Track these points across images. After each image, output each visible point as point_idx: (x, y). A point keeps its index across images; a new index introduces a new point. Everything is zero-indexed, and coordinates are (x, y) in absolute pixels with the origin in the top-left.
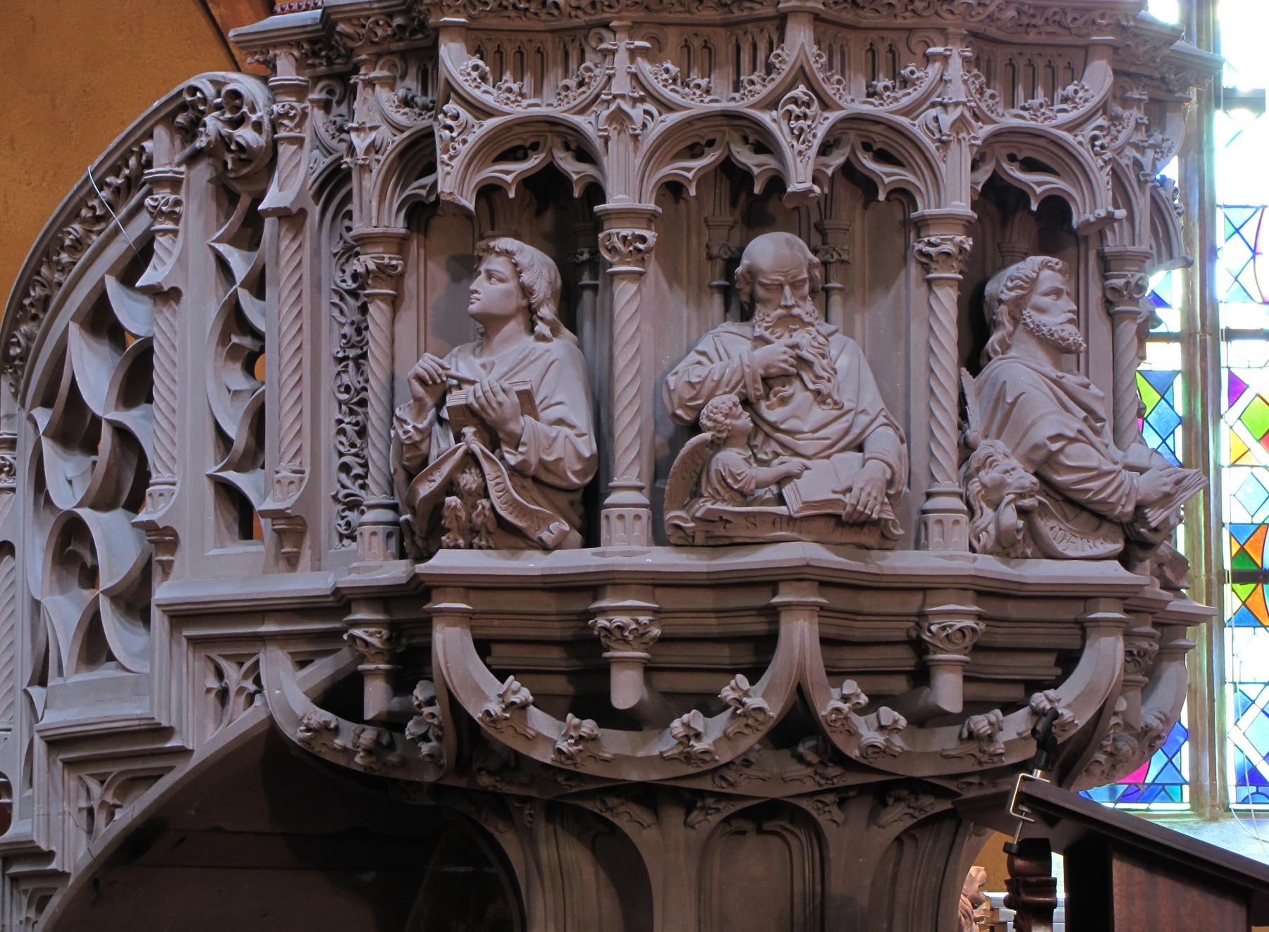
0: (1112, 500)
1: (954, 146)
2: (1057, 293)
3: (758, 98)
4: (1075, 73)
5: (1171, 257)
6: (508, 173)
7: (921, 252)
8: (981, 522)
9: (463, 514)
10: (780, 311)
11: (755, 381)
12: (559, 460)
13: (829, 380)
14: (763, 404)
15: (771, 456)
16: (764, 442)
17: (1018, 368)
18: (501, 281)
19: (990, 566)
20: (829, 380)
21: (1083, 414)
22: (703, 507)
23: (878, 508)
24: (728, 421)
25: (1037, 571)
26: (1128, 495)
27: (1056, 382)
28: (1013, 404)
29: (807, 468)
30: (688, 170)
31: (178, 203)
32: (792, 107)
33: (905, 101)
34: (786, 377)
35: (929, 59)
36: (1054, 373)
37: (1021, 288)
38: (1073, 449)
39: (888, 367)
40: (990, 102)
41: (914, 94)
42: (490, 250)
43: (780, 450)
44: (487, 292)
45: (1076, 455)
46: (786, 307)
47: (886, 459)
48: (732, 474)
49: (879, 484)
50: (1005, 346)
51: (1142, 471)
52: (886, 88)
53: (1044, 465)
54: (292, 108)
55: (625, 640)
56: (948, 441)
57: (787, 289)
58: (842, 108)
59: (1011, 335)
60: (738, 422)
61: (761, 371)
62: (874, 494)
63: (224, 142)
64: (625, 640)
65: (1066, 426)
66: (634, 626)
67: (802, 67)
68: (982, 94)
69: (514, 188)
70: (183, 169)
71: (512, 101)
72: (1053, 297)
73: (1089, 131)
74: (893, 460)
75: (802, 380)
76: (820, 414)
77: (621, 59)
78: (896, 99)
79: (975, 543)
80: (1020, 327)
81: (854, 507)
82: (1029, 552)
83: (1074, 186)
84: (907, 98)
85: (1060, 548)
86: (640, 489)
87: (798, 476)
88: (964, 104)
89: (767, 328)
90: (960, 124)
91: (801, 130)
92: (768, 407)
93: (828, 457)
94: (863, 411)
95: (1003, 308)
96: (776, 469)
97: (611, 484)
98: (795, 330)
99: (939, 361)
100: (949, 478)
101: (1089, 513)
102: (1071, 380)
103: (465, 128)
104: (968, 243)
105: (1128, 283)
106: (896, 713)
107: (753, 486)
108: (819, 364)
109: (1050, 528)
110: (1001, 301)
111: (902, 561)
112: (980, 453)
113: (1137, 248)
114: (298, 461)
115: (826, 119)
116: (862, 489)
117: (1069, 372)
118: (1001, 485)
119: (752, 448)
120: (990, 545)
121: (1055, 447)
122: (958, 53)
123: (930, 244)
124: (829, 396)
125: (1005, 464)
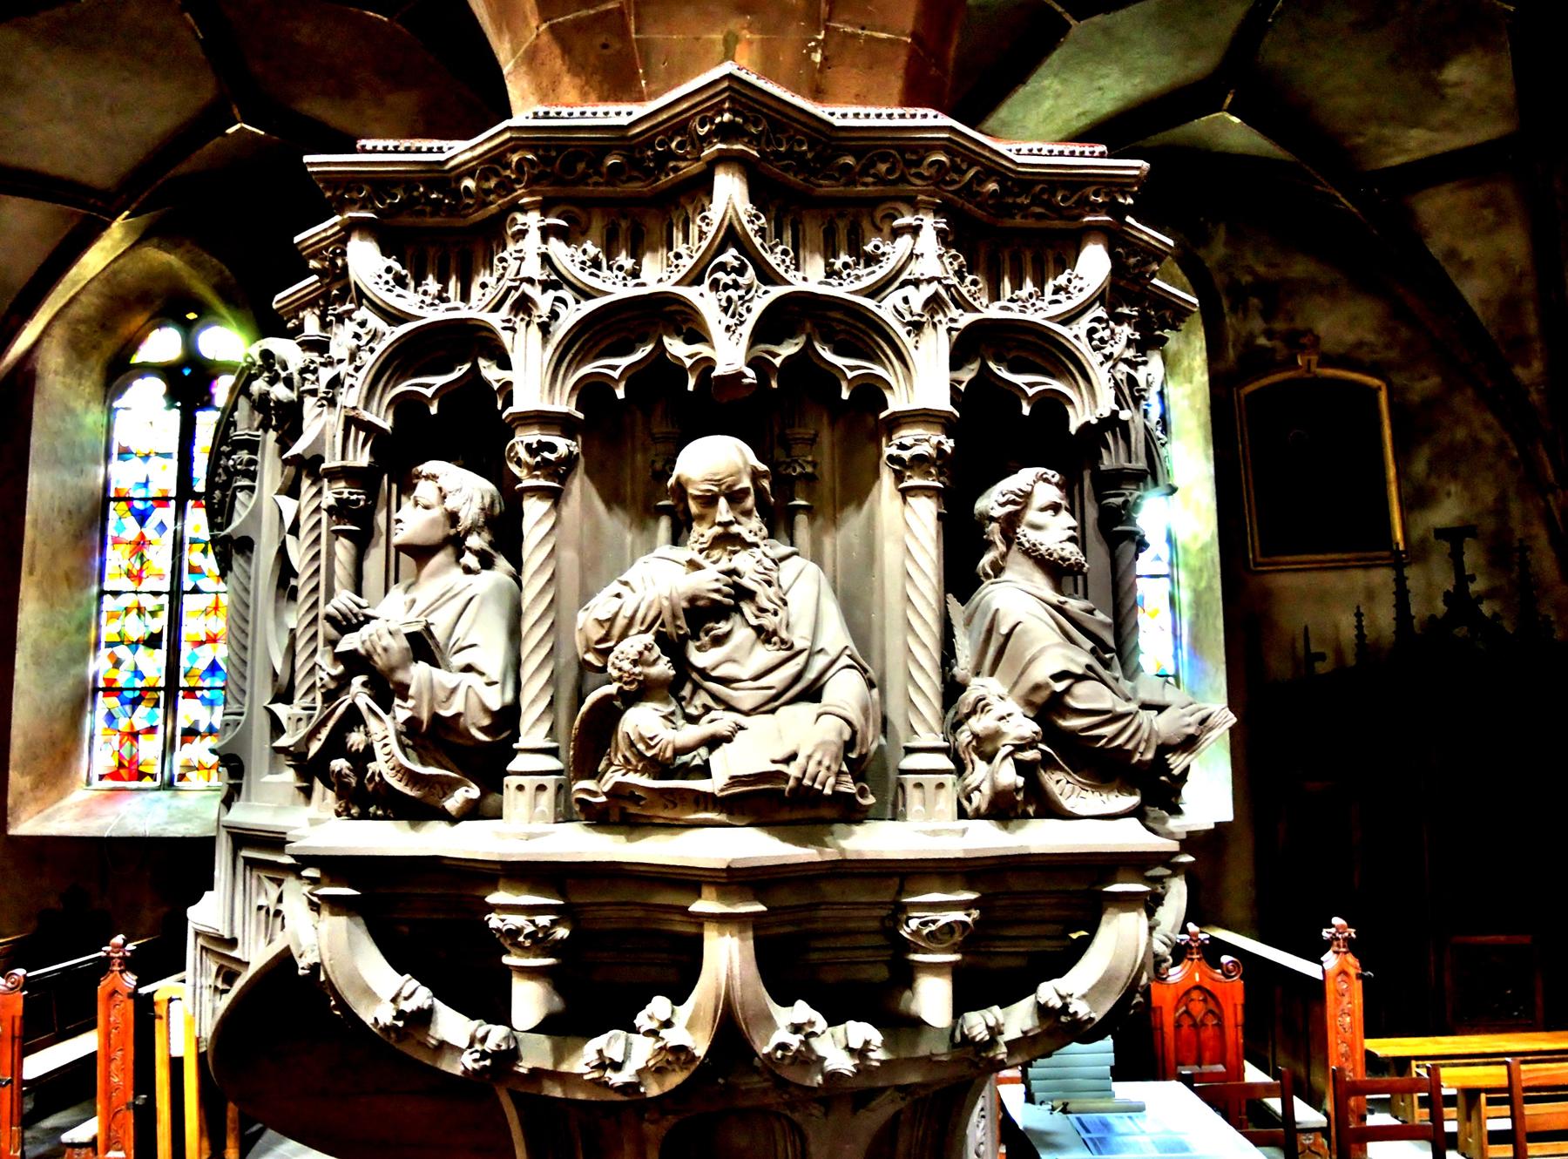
0: (1130, 746)
1: (928, 330)
2: (1055, 508)
3: (684, 271)
4: (1066, 260)
5: (1156, 483)
6: (428, 386)
7: (891, 458)
8: (972, 779)
9: (353, 781)
10: (718, 530)
11: (675, 616)
12: (459, 715)
13: (776, 613)
14: (692, 646)
15: (701, 710)
16: (694, 693)
17: (1015, 595)
18: (427, 508)
19: (987, 839)
20: (776, 613)
21: (1089, 645)
22: (613, 777)
23: (831, 781)
24: (638, 670)
25: (1038, 837)
26: (1148, 741)
27: (1059, 609)
28: (1008, 636)
29: (742, 728)
30: (614, 368)
31: (254, 462)
32: (720, 275)
33: (867, 281)
34: (719, 611)
35: (896, 233)
36: (1055, 598)
37: (1013, 502)
38: (1081, 689)
39: (856, 601)
40: (973, 288)
41: (880, 272)
42: (418, 476)
43: (711, 703)
44: (413, 520)
45: (1088, 695)
46: (720, 524)
47: (843, 713)
48: (642, 738)
49: (834, 749)
50: (998, 569)
51: (1161, 708)
52: (846, 266)
53: (1048, 707)
54: (313, 362)
55: (520, 946)
56: (930, 683)
57: (723, 502)
58: (789, 283)
59: (1004, 556)
60: (654, 671)
61: (685, 604)
62: (826, 762)
63: (265, 396)
64: (520, 946)
65: (1072, 660)
66: (530, 928)
67: (731, 225)
68: (962, 279)
69: (436, 403)
70: (260, 432)
71: (425, 304)
72: (1050, 512)
73: (1084, 324)
74: (855, 715)
75: (742, 615)
76: (766, 655)
77: (534, 236)
78: (858, 278)
79: (965, 803)
80: (1015, 547)
81: (799, 780)
82: (1031, 810)
83: (1071, 386)
84: (870, 276)
85: (1068, 804)
86: (553, 752)
87: (728, 739)
88: (939, 280)
89: (701, 551)
90: (934, 304)
91: (729, 300)
92: (699, 649)
93: (773, 711)
94: (821, 651)
95: (994, 527)
96: (703, 729)
97: (515, 746)
98: (735, 552)
99: (916, 587)
100: (931, 730)
101: (1103, 765)
102: (1075, 605)
103: (375, 336)
104: (949, 445)
105: (1126, 502)
106: (1097, 19)
107: (669, 754)
108: (764, 595)
109: (1060, 785)
110: (992, 519)
111: (870, 841)
112: (969, 696)
113: (1134, 465)
114: (310, 698)
115: (766, 292)
116: (809, 757)
117: (1070, 596)
118: (997, 735)
119: (680, 700)
120: (984, 807)
121: (1059, 687)
122: (930, 224)
123: (902, 447)
124: (775, 633)
125: (999, 708)
